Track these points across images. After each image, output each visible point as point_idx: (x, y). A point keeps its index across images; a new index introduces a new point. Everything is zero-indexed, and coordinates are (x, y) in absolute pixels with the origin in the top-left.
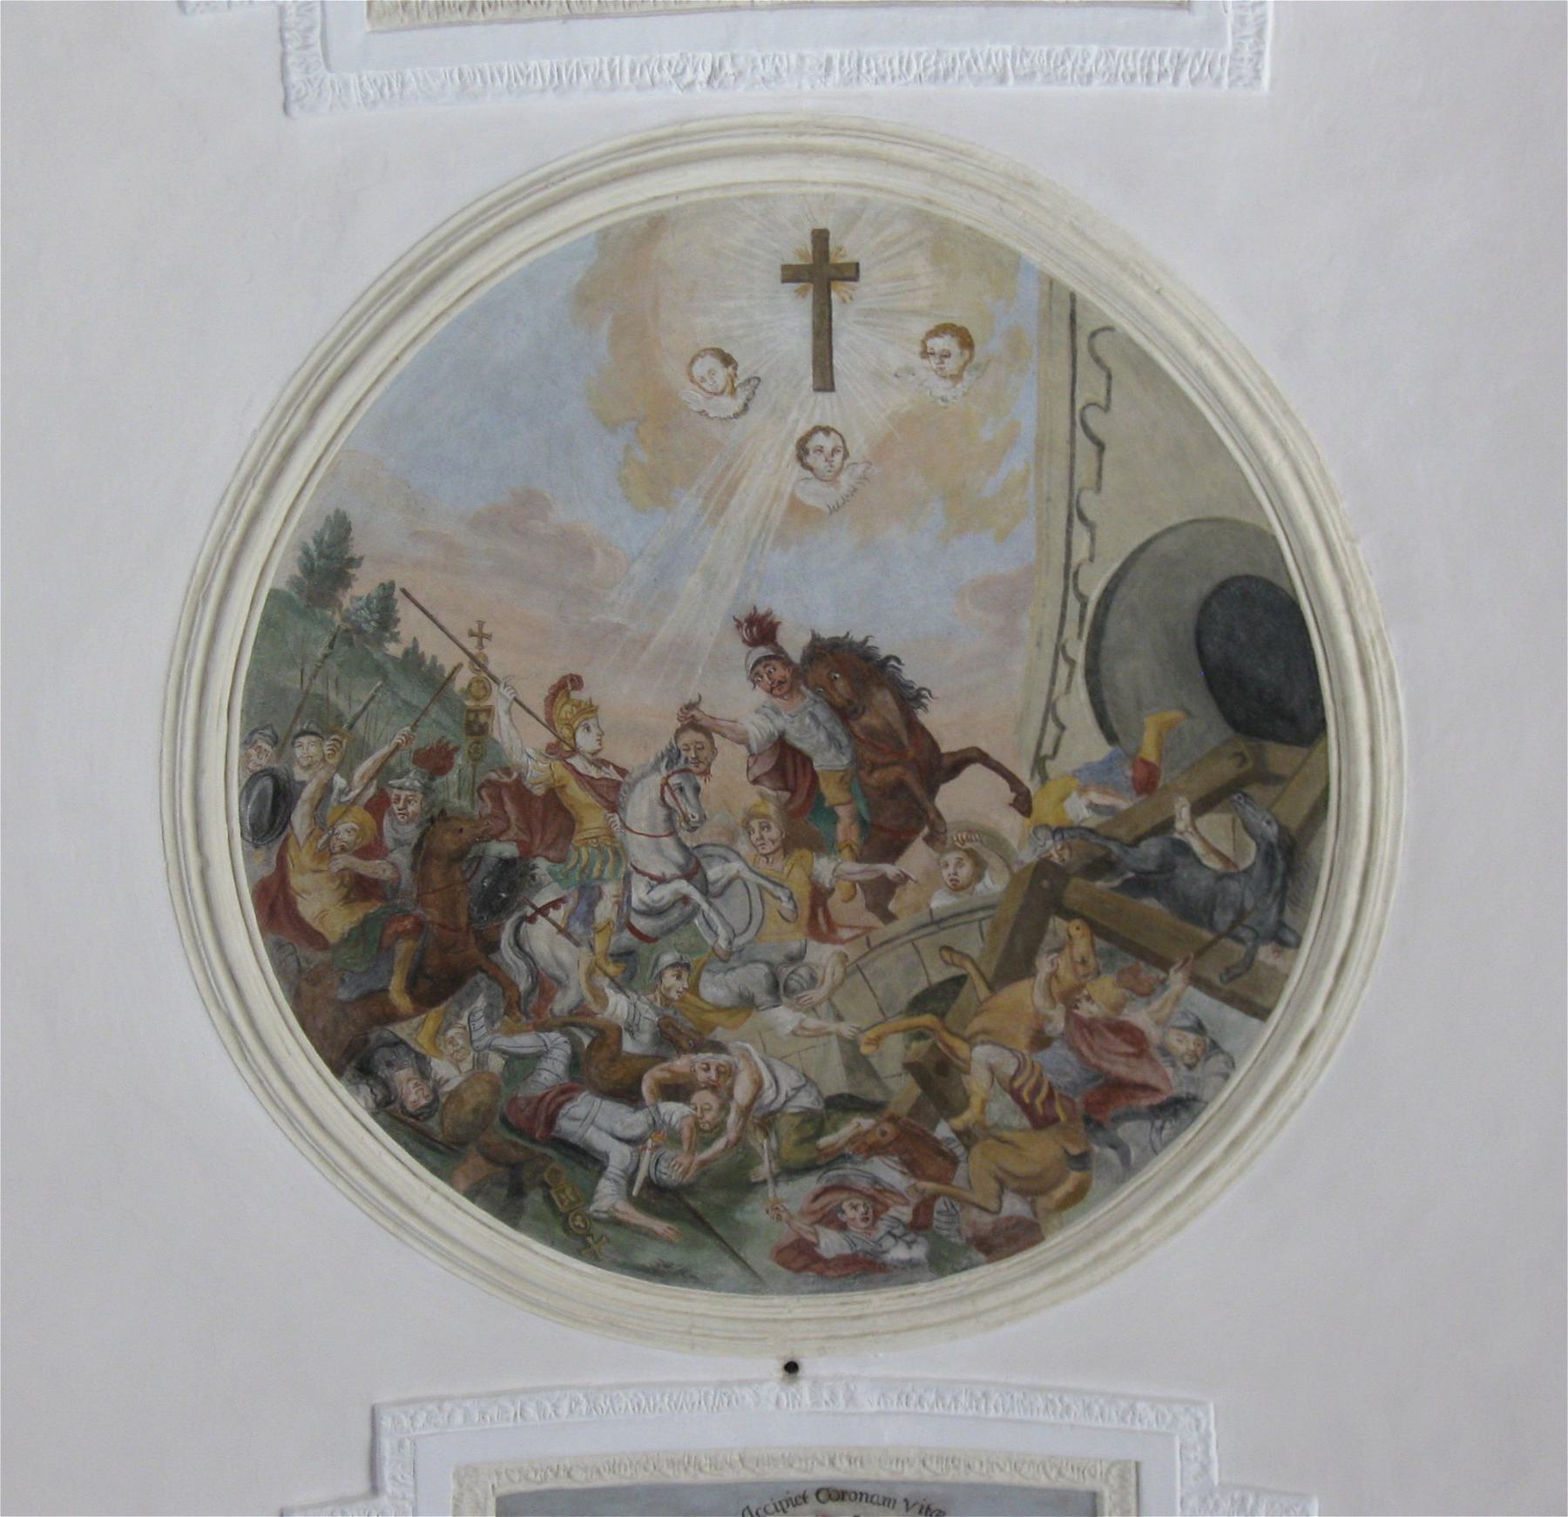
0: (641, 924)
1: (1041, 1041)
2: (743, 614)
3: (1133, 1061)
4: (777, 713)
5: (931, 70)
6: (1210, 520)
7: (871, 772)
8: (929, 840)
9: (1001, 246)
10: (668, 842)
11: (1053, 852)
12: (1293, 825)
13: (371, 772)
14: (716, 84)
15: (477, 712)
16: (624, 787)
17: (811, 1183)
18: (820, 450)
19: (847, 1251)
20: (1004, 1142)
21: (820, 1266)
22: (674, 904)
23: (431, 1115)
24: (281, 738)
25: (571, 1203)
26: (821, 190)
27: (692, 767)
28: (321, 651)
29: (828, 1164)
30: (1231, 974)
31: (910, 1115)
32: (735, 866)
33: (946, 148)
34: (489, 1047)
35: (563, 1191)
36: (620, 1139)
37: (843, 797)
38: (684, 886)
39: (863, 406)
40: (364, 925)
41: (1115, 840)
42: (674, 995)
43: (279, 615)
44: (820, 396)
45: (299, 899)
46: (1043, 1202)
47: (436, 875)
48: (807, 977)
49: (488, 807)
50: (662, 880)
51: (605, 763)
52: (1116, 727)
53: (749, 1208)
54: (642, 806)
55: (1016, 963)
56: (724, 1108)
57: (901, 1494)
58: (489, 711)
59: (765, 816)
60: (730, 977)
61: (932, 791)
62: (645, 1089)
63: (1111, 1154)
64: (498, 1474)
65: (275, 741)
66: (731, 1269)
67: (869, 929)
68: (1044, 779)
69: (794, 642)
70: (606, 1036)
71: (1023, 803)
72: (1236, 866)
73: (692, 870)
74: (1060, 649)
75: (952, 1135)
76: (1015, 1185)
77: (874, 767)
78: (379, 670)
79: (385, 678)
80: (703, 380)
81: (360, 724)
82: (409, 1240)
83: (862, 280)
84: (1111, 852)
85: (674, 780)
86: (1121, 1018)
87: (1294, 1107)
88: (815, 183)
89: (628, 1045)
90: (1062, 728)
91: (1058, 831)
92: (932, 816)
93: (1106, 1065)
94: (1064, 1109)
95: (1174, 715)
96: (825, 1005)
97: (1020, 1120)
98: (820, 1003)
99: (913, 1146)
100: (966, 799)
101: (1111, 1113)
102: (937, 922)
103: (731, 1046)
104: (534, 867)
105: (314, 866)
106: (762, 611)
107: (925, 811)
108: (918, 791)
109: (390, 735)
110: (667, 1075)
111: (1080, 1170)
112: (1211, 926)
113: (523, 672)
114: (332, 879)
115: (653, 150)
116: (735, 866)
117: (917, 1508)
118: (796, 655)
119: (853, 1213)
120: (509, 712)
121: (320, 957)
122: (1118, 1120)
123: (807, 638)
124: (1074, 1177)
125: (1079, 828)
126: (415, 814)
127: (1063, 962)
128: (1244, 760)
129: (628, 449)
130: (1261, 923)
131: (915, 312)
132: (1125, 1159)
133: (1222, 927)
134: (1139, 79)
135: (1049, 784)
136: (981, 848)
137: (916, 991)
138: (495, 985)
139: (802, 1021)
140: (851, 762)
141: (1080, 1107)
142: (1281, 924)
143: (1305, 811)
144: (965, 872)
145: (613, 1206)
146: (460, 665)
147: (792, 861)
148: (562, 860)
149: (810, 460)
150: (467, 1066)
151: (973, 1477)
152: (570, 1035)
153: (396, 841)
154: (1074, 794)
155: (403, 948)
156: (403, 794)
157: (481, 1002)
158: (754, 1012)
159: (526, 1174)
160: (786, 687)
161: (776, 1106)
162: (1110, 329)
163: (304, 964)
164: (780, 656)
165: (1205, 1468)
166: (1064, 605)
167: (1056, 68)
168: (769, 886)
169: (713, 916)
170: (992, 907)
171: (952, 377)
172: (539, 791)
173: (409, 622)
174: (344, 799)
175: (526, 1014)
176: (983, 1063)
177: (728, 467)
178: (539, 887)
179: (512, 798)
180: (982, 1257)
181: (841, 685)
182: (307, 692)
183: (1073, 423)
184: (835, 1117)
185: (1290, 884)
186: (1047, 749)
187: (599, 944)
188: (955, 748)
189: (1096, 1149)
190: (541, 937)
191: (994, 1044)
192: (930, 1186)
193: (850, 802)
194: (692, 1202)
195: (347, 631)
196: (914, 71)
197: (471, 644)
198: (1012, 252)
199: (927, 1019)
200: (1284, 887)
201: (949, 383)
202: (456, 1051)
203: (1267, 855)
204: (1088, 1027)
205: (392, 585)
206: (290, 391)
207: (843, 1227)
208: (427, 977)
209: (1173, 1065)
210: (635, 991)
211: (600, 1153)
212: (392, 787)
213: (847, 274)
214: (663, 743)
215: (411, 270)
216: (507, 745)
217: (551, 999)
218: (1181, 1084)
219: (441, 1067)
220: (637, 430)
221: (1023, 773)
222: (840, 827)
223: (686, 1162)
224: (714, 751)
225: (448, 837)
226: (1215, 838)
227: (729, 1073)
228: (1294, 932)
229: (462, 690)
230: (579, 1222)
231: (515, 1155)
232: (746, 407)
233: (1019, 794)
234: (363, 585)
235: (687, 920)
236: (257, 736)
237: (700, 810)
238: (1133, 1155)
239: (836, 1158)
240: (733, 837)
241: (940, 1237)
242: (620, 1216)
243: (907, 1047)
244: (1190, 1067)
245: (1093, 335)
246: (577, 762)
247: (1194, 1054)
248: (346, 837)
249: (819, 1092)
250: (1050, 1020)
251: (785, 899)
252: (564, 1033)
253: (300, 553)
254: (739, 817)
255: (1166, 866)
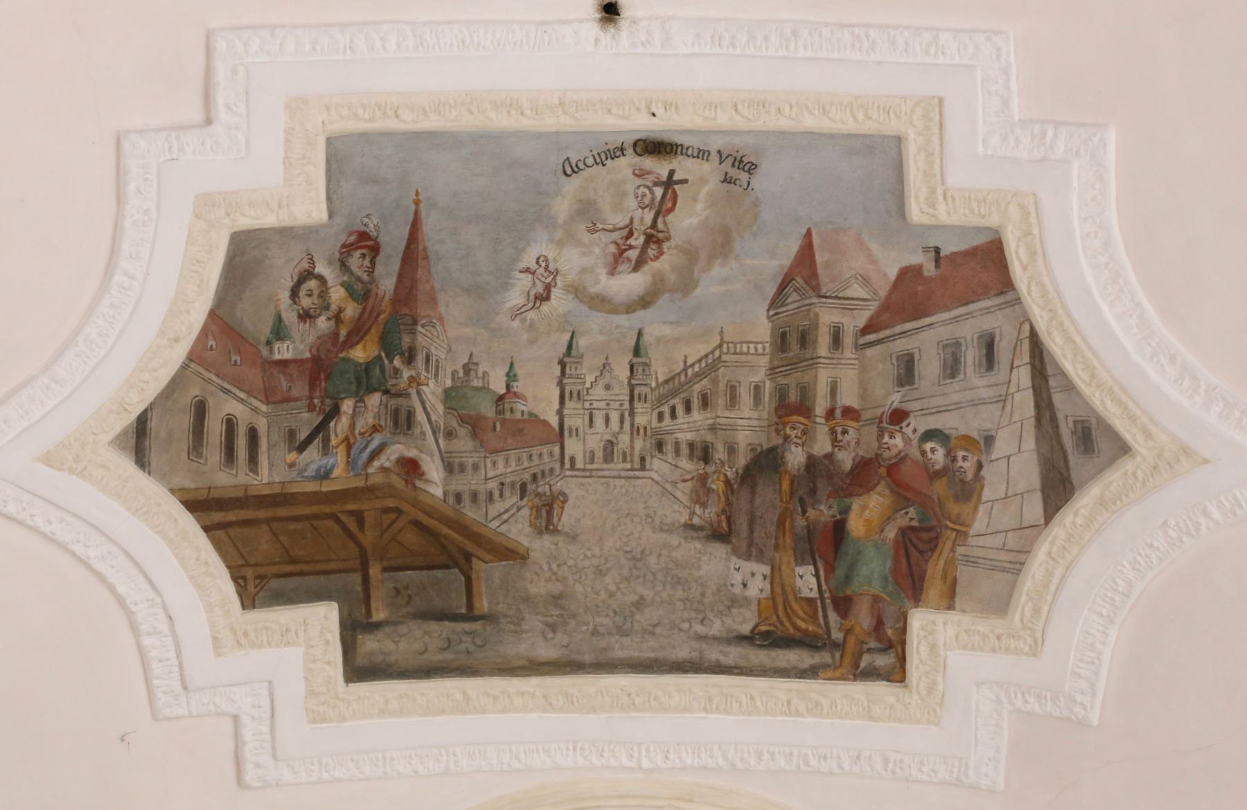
5: (643, 748)
57: (715, 145)
64: (328, 108)
117: (730, 160)
151: (784, 123)
165: (1006, 103)
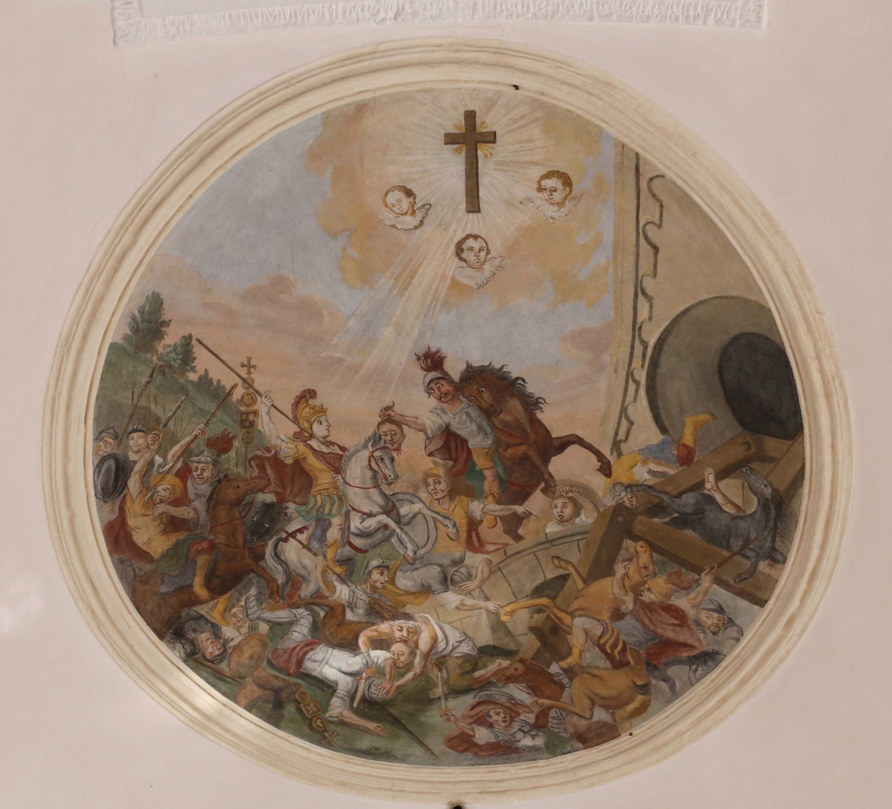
0: (358, 542)
1: (618, 615)
2: (421, 351)
3: (678, 629)
4: (445, 413)
6: (727, 297)
7: (506, 449)
8: (544, 491)
9: (589, 123)
10: (374, 492)
11: (625, 499)
12: (782, 488)
13: (179, 454)
14: (400, 19)
15: (248, 414)
16: (345, 458)
17: (469, 699)
18: (471, 249)
19: (493, 740)
20: (595, 676)
21: (475, 749)
22: (378, 529)
23: (222, 661)
24: (120, 435)
25: (314, 712)
26: (471, 86)
27: (389, 446)
28: (144, 380)
29: (480, 687)
30: (740, 578)
31: (533, 658)
32: (418, 506)
33: (554, 60)
34: (259, 618)
35: (309, 705)
36: (344, 673)
37: (488, 464)
38: (384, 519)
39: (498, 222)
40: (176, 546)
41: (666, 493)
42: (379, 585)
43: (116, 359)
44: (471, 215)
45: (134, 533)
46: (620, 713)
47: (223, 514)
48: (466, 574)
49: (256, 473)
50: (370, 515)
51: (332, 444)
52: (666, 424)
53: (429, 714)
54: (356, 469)
55: (601, 567)
56: (413, 654)
58: (255, 413)
59: (436, 476)
60: (415, 573)
61: (546, 461)
62: (361, 641)
63: (663, 685)
65: (116, 437)
66: (418, 751)
67: (506, 545)
68: (620, 454)
69: (455, 369)
70: (335, 611)
71: (606, 469)
72: (744, 512)
73: (390, 509)
74: (630, 375)
75: (561, 671)
76: (601, 702)
77: (508, 446)
78: (183, 390)
79: (187, 395)
80: (394, 206)
81: (171, 423)
82: (210, 736)
83: (498, 143)
84: (663, 500)
85: (377, 454)
86: (670, 602)
87: (782, 660)
88: (465, 81)
89: (349, 616)
90: (632, 423)
91: (628, 487)
92: (546, 476)
93: (659, 631)
94: (632, 656)
95: (703, 417)
96: (477, 591)
97: (603, 663)
98: (474, 590)
99: (535, 677)
100: (567, 466)
101: (664, 660)
102: (550, 541)
103: (416, 616)
104: (287, 508)
105: (143, 512)
106: (433, 350)
107: (542, 473)
108: (538, 461)
109: (190, 430)
110: (375, 634)
111: (642, 694)
112: (728, 547)
113: (277, 387)
114: (154, 520)
115: (359, 62)
116: (418, 506)
118: (456, 377)
119: (497, 717)
120: (268, 413)
121: (148, 567)
122: (668, 664)
123: (463, 367)
124: (640, 698)
125: (643, 485)
126: (208, 478)
127: (632, 568)
128: (750, 447)
129: (344, 249)
130: (761, 548)
131: (534, 163)
132: (673, 688)
133: (736, 549)
134: (681, 20)
135: (623, 458)
136: (578, 496)
137: (536, 583)
138: (262, 581)
139: (463, 600)
140: (493, 443)
141: (644, 656)
142: (773, 549)
143: (789, 480)
144: (568, 511)
145: (341, 713)
146: (236, 385)
147: (456, 502)
148: (305, 504)
149: (464, 255)
150: (244, 630)
152: (312, 610)
153: (196, 494)
154: (639, 464)
155: (202, 560)
156: (200, 466)
157: (253, 591)
158: (431, 595)
159: (284, 695)
160: (450, 397)
161: (444, 653)
162: (662, 176)
163: (137, 572)
164: (446, 377)
166: (632, 347)
167: (626, 11)
168: (440, 518)
169: (403, 536)
170: (586, 533)
171: (558, 204)
172: (289, 461)
173: (203, 360)
174: (161, 470)
175: (282, 597)
176: (580, 629)
177: (411, 260)
178: (290, 520)
179: (271, 466)
180: (580, 745)
181: (486, 395)
182: (136, 405)
183: (638, 234)
184: (484, 659)
185: (779, 524)
186: (622, 435)
187: (330, 554)
188: (562, 435)
189: (654, 681)
190: (292, 551)
191: (587, 616)
192: (547, 702)
193: (492, 468)
194: (392, 711)
195: (161, 366)
196: (532, 11)
197: (243, 372)
198: (598, 127)
199: (543, 601)
200: (775, 527)
201: (556, 208)
202: (236, 622)
203: (765, 505)
204: (649, 607)
205: (190, 337)
206: (121, 219)
207: (490, 726)
208: (217, 577)
209: (704, 632)
210: (354, 583)
211: (332, 681)
212: (192, 461)
213: (488, 139)
214: (370, 432)
215: (199, 141)
216: (268, 434)
217: (299, 589)
218: (708, 644)
219: (228, 632)
220: (350, 237)
221: (606, 451)
222: (486, 483)
223: (388, 686)
224: (403, 436)
225: (230, 491)
226: (731, 495)
227: (416, 632)
228: (782, 554)
229: (237, 400)
230: (319, 723)
231: (277, 684)
232: (422, 223)
233: (603, 464)
234: (172, 337)
235: (387, 539)
236: (104, 434)
237: (394, 471)
238: (678, 685)
239: (485, 684)
240: (417, 488)
241: (553, 733)
242: (345, 719)
243: (531, 617)
244: (714, 634)
245: (651, 179)
246: (314, 443)
247: (717, 626)
248: (163, 493)
249: (474, 644)
250: (624, 603)
251: (450, 526)
252: (307, 610)
253: (129, 320)
254: (420, 476)
255: (699, 511)
